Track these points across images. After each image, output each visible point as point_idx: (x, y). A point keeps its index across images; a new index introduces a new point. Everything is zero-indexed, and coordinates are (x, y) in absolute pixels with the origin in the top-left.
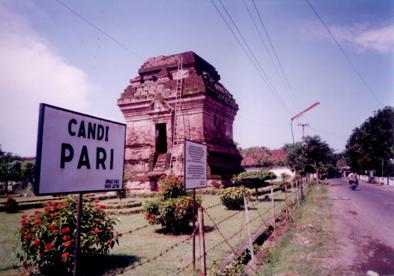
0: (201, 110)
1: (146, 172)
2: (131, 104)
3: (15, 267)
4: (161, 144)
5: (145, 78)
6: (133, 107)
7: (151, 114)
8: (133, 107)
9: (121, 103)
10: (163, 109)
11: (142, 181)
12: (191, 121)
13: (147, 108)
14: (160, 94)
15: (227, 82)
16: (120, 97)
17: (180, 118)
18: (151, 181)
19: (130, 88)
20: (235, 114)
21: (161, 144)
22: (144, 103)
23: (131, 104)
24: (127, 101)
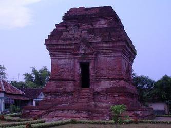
2: (57, 45)
4: (85, 80)
5: (69, 23)
10: (88, 51)
20: (134, 58)
21: (85, 80)
23: (57, 45)
24: (54, 42)
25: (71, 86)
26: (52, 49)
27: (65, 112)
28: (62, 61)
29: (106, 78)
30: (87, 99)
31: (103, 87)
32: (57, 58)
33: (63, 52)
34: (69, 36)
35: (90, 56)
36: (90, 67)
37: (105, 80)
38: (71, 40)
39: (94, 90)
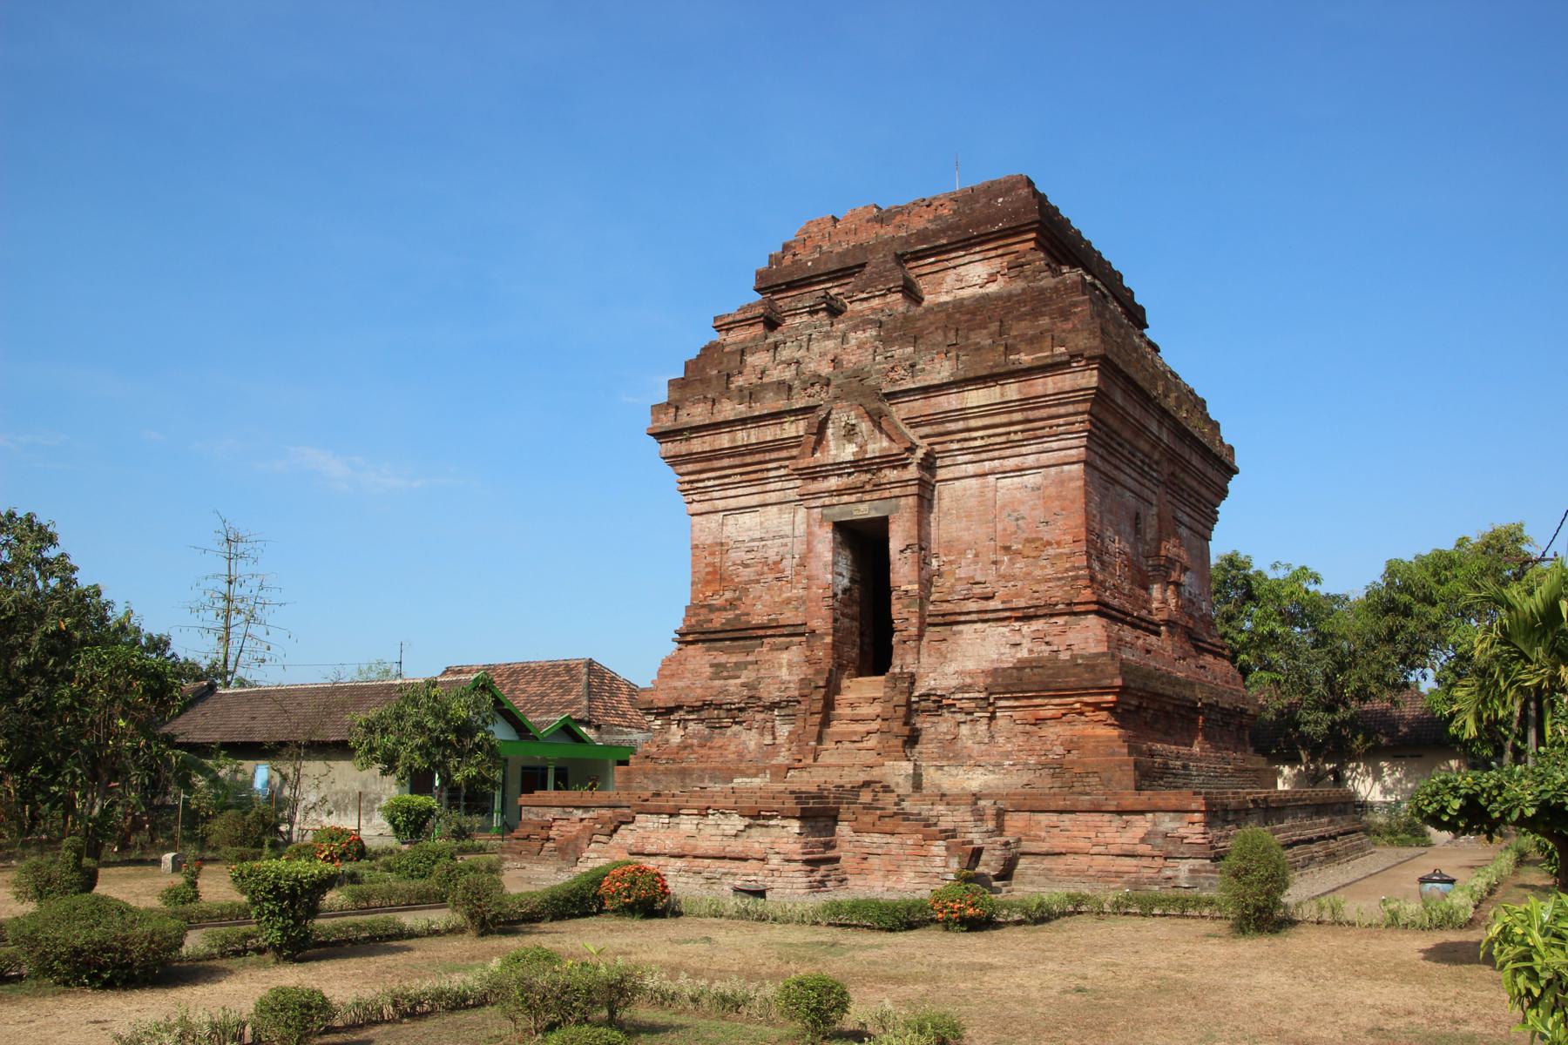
0: (1073, 447)
1: (781, 772)
2: (715, 427)
3: (1059, 543)
4: (868, 626)
5: (784, 301)
6: (724, 440)
7: (812, 474)
8: (724, 440)
9: (667, 422)
10: (878, 446)
11: (757, 816)
12: (1007, 506)
13: (797, 441)
14: (859, 375)
15: (1185, 346)
16: (663, 396)
17: (962, 489)
18: (806, 817)
19: (710, 350)
20: (1222, 493)
21: (868, 626)
22: (777, 416)
23: (715, 427)
24: (697, 414)
25: (790, 665)
26: (690, 458)
27: (687, 824)
28: (747, 519)
29: (992, 604)
30: (872, 742)
31: (971, 665)
32: (720, 504)
33: (750, 463)
34: (775, 375)
35: (892, 475)
36: (895, 545)
37: (985, 617)
38: (785, 388)
39: (912, 679)
